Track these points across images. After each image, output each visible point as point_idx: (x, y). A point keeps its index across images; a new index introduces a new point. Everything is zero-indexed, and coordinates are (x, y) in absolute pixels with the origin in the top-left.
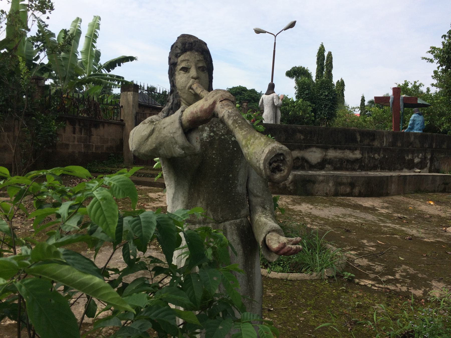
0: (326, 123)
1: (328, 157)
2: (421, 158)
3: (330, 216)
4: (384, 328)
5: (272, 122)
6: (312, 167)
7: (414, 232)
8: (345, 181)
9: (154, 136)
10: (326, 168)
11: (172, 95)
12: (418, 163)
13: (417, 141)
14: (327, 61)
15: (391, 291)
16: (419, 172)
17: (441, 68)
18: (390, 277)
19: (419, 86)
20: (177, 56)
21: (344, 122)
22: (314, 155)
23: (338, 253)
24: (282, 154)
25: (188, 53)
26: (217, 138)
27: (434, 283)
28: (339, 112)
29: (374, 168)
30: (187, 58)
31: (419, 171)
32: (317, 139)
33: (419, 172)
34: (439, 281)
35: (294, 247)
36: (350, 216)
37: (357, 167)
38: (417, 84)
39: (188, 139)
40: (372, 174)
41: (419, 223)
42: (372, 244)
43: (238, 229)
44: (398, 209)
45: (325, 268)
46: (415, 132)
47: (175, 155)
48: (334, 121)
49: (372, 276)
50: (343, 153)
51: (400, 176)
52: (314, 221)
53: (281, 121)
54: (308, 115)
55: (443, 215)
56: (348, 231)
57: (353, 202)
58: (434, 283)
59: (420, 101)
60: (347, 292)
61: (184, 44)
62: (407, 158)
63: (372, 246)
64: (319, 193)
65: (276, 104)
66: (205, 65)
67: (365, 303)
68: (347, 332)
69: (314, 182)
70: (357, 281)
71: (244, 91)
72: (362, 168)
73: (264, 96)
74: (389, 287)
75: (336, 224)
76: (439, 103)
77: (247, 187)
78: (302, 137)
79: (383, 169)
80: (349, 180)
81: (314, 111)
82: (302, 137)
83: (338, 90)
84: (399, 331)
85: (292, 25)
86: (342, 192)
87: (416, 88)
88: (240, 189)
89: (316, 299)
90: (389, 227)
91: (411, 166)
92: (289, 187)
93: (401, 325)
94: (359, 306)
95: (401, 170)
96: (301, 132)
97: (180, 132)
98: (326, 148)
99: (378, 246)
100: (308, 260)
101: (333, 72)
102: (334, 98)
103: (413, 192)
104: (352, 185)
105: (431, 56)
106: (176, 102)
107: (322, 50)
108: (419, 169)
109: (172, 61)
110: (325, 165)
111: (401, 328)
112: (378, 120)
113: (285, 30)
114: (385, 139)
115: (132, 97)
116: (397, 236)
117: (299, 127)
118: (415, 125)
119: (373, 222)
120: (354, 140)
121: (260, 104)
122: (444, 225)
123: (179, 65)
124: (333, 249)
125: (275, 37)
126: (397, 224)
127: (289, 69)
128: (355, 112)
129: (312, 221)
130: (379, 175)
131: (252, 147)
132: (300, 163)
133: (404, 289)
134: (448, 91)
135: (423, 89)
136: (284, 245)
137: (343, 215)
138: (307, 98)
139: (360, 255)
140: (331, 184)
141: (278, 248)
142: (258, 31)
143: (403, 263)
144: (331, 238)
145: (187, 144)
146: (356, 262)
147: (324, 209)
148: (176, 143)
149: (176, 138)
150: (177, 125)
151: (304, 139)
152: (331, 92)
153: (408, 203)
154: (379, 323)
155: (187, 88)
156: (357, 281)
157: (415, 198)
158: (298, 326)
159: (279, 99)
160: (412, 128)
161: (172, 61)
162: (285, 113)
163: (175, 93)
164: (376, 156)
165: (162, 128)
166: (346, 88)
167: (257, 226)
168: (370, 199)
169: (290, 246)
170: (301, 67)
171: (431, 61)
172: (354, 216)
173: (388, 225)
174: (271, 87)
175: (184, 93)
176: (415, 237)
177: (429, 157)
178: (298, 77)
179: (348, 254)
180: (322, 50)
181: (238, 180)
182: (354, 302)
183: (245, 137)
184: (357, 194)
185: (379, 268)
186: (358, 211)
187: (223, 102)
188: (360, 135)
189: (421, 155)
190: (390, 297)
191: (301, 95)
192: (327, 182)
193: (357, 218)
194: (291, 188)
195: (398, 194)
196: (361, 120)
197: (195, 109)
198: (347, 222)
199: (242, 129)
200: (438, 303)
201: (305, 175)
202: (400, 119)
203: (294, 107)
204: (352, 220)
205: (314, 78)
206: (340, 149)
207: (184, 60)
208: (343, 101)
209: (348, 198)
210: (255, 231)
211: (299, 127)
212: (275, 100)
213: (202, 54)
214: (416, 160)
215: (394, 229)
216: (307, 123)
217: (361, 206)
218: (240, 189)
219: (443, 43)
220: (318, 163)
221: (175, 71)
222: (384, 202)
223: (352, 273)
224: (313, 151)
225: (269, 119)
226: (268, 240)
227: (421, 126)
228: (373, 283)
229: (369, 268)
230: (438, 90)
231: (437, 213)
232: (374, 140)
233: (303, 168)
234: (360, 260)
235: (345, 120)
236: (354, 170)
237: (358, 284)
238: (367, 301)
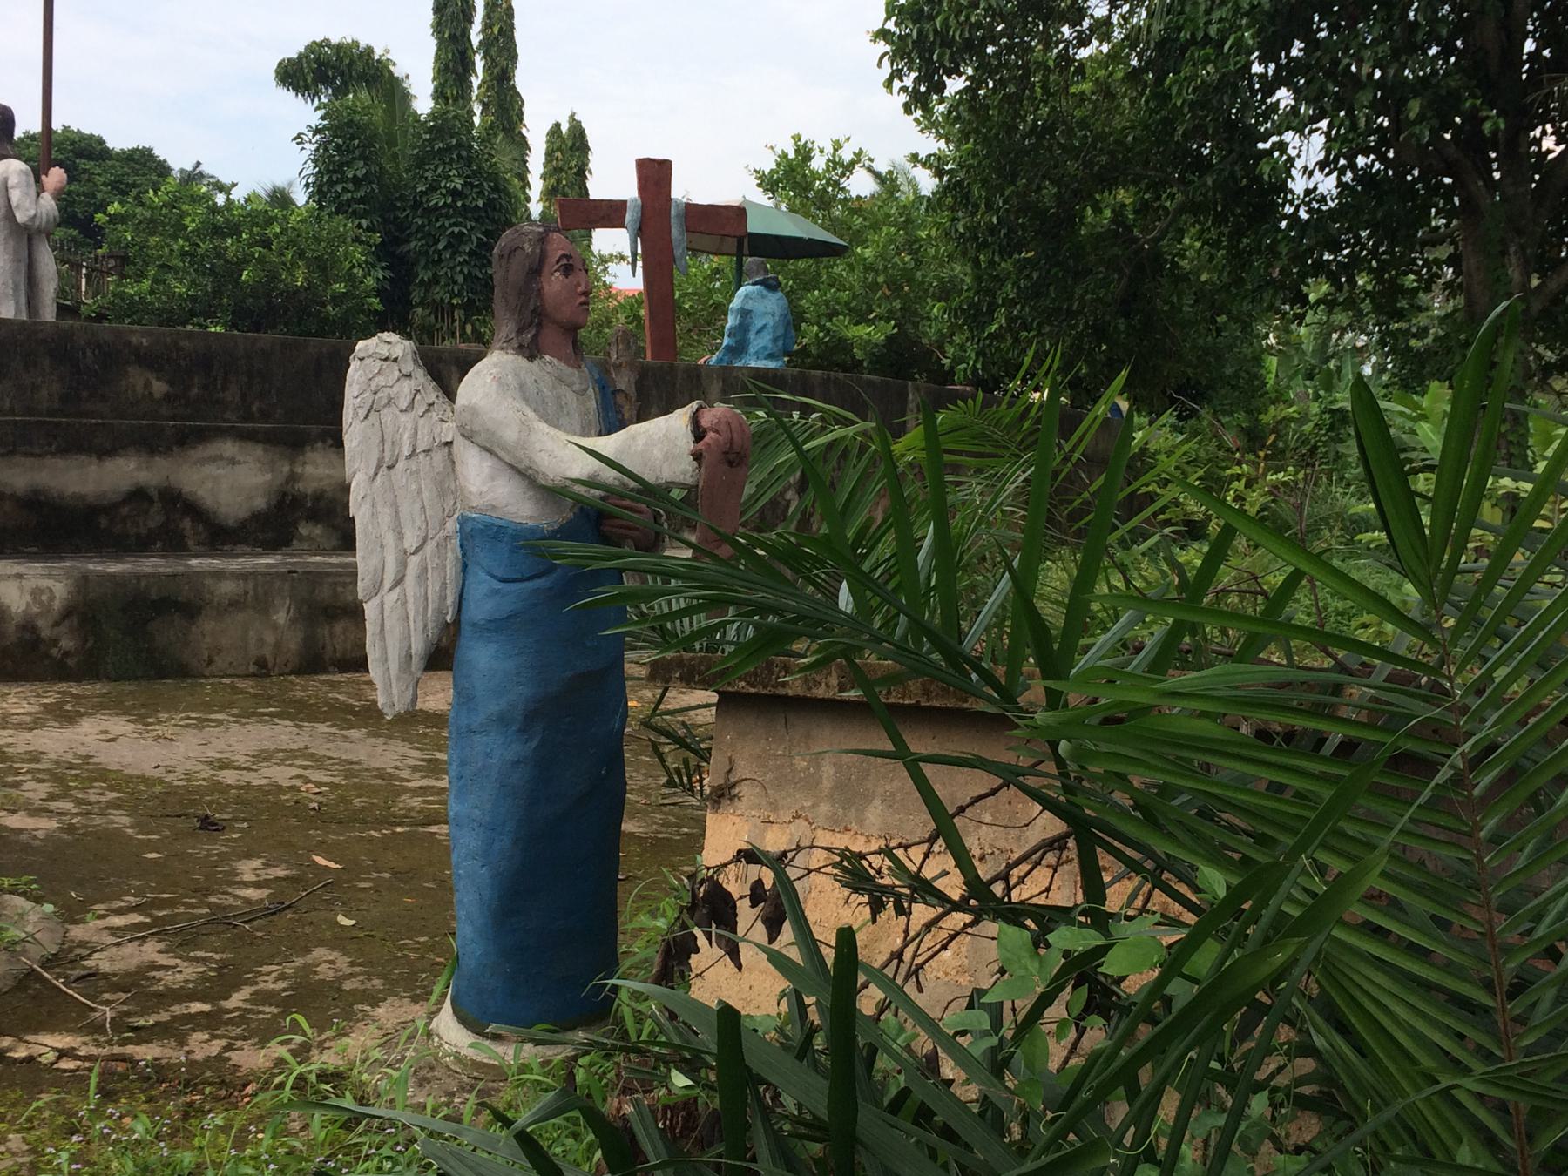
0: (463, 328)
1: (307, 487)
6: (220, 536)
10: (301, 539)
14: (487, 26)
32: (243, 397)
46: (753, 364)
54: (340, 287)
64: (220, 662)
65: (20, 217)
69: (191, 610)
71: (90, 157)
78: (159, 387)
92: (55, 642)
96: (148, 360)
101: (523, 79)
102: (490, 204)
110: (295, 525)
118: (752, 336)
127: (293, 49)
132: (155, 519)
138: (361, 201)
140: (281, 617)
151: (167, 397)
152: (475, 174)
160: (739, 349)
170: (356, 44)
178: (339, 93)
194: (67, 643)
205: (423, 104)
220: (256, 517)
224: (221, 458)
227: (775, 340)
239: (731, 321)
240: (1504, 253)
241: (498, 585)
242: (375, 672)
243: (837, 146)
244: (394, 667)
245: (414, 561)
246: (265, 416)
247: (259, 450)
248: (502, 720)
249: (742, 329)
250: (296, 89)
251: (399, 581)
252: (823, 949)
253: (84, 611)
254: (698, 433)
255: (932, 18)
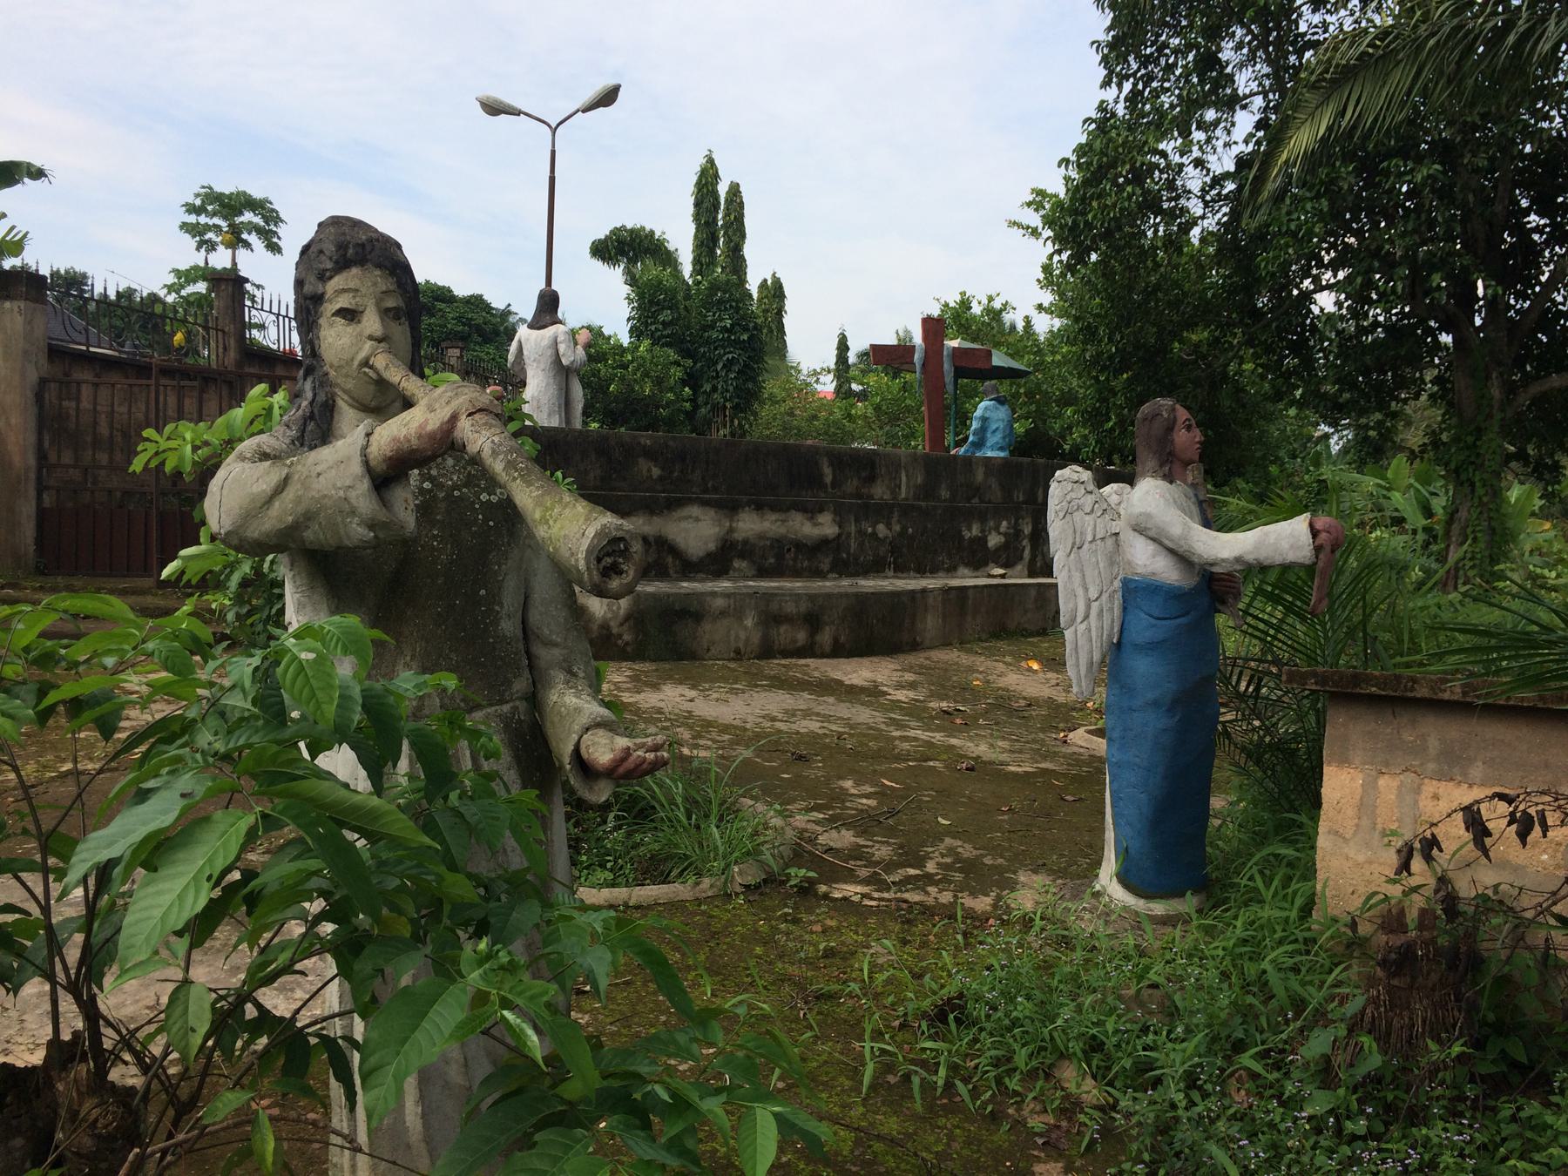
1: (739, 536)
2: (1005, 535)
3: (750, 719)
4: (891, 999)
5: (555, 422)
6: (690, 568)
7: (982, 749)
8: (790, 608)
9: (290, 494)
10: (735, 570)
11: (309, 380)
12: (998, 549)
13: (994, 483)
14: (727, 215)
15: (911, 905)
16: (1003, 576)
17: (1056, 258)
18: (912, 872)
19: (1001, 311)
20: (323, 277)
21: (787, 418)
22: (696, 530)
23: (777, 822)
24: (621, 539)
25: (355, 271)
26: (442, 495)
27: (1022, 877)
28: (771, 386)
29: (875, 568)
30: (352, 285)
31: (1001, 571)
33: (1003, 576)
34: (1035, 872)
35: (651, 756)
36: (807, 714)
37: (825, 566)
38: (997, 305)
39: (384, 503)
40: (869, 584)
41: (997, 724)
42: (868, 789)
43: (507, 727)
44: (943, 687)
45: (736, 863)
46: (989, 454)
47: (347, 543)
48: (755, 414)
49: (864, 873)
50: (783, 521)
51: (947, 591)
52: (701, 737)
53: (586, 413)
55: (1061, 698)
56: (800, 758)
57: (816, 674)
58: (1022, 877)
59: (999, 359)
60: (796, 921)
61: (342, 247)
62: (967, 535)
63: (867, 796)
65: (565, 362)
66: (402, 304)
67: (843, 943)
68: (797, 1020)
70: (823, 888)
72: (844, 568)
73: (523, 332)
74: (906, 896)
75: (771, 744)
76: (1059, 364)
77: (524, 622)
78: (656, 472)
79: (900, 569)
80: (804, 607)
81: (691, 379)
82: (656, 472)
83: (766, 311)
84: (929, 1000)
85: (608, 97)
86: (785, 641)
87: (995, 315)
88: (509, 627)
89: (711, 949)
90: (916, 739)
91: (978, 557)
92: (620, 636)
93: (935, 987)
94: (829, 953)
95: (951, 570)
96: (650, 454)
97: (365, 485)
98: (729, 508)
99: (882, 794)
100: (685, 845)
101: (748, 251)
103: (984, 636)
104: (813, 621)
105: (1035, 219)
106: (321, 397)
107: (708, 177)
108: (1001, 567)
109: (307, 289)
111: (935, 993)
112: (889, 415)
113: (584, 111)
114: (904, 479)
115: (19, 319)
116: (937, 764)
117: (646, 438)
119: (871, 728)
120: (815, 481)
121: (511, 357)
122: (1061, 725)
123: (330, 301)
124: (758, 810)
125: (554, 131)
126: (939, 729)
128: (819, 387)
129: (694, 738)
130: (890, 588)
131: (558, 525)
133: (946, 897)
134: (1081, 330)
135: (1016, 318)
136: (627, 752)
137: (786, 712)
139: (834, 822)
140: (749, 622)
141: (613, 761)
142: (494, 108)
143: (949, 832)
144: (745, 776)
145: (382, 515)
146: (822, 840)
147: (732, 698)
148: (353, 512)
149: (353, 501)
150: (356, 467)
151: (661, 478)
153: (971, 669)
154: (879, 990)
155: (356, 363)
156: (823, 888)
157: (990, 653)
158: (665, 1023)
159: (576, 344)
160: (979, 444)
161: (307, 289)
162: (596, 387)
163: (318, 373)
164: (881, 529)
165: (314, 474)
166: (789, 305)
167: (556, 719)
168: (866, 661)
169: (640, 753)
170: (643, 228)
171: (1035, 233)
172: (818, 714)
173: (912, 733)
174: (548, 305)
175: (347, 376)
176: (985, 763)
177: (1027, 530)
178: (632, 261)
179: (800, 820)
180: (708, 177)
181: (501, 604)
182: (815, 945)
183: (539, 502)
184: (828, 649)
185: (882, 852)
186: (831, 700)
187: (477, 416)
188: (831, 464)
189: (1004, 523)
190: (908, 922)
191: (647, 325)
192: (739, 614)
193: (827, 718)
194: (627, 637)
195: (946, 644)
196: (838, 414)
197: (404, 431)
198: (798, 733)
199: (529, 484)
200: (1027, 922)
201: (669, 595)
202: (949, 415)
203: (625, 367)
204: (814, 726)
205: (687, 269)
206: (774, 508)
207: (344, 291)
208: (782, 349)
209: (802, 661)
210: (550, 731)
211: (646, 438)
212: (562, 348)
213: (392, 274)
214: (994, 540)
215: (929, 744)
216: (670, 424)
217: (840, 683)
218: (509, 627)
219: (1067, 179)
220: (709, 555)
221: (318, 315)
222: (903, 670)
223: (809, 869)
225: (545, 410)
226: (587, 747)
228: (866, 889)
229: (856, 853)
230: (1057, 323)
231: (1045, 692)
232: (871, 479)
233: (661, 573)
234: (834, 834)
235: (791, 414)
236: (819, 574)
237: (826, 896)
238: (851, 937)
239: (975, 425)
240: (1488, 378)
241: (1153, 621)
242: (1071, 671)
243: (991, 299)
244: (1083, 671)
245: (1095, 605)
246: (715, 490)
247: (712, 512)
248: (1155, 704)
249: (982, 430)
250: (604, 260)
251: (1086, 617)
252: (356, 836)
253: (636, 618)
254: (1315, 533)
255: (1085, 214)
